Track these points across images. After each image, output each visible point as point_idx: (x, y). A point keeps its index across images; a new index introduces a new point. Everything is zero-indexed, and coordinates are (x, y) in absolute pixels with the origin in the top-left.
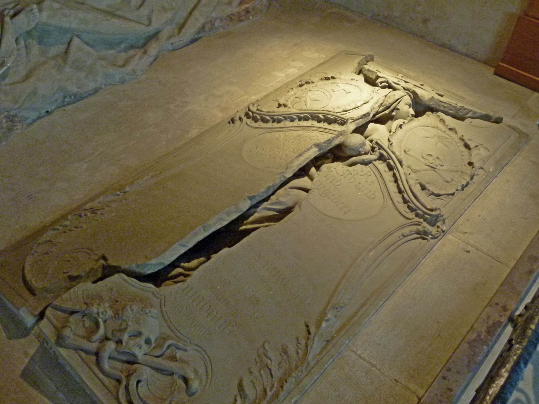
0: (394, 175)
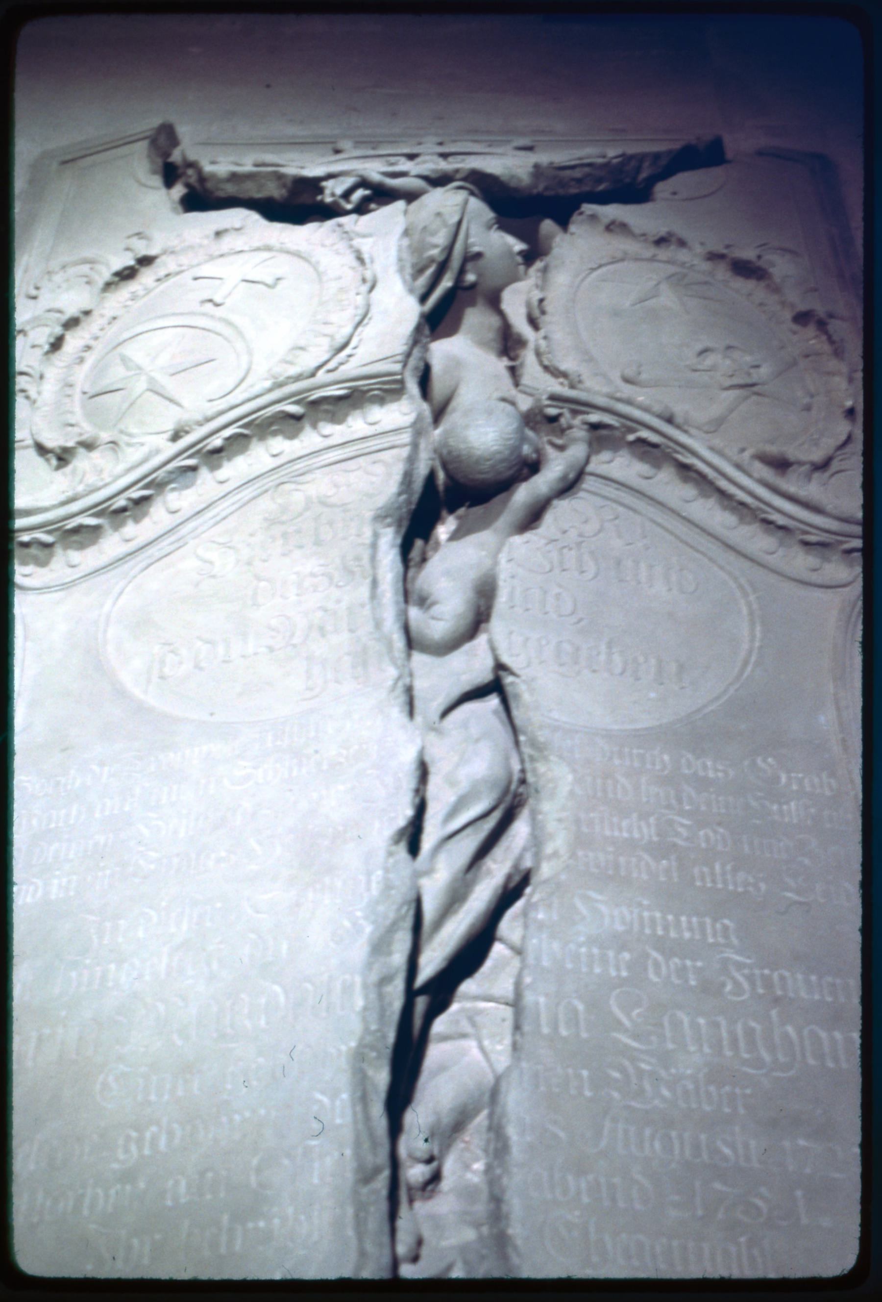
0: (684, 469)
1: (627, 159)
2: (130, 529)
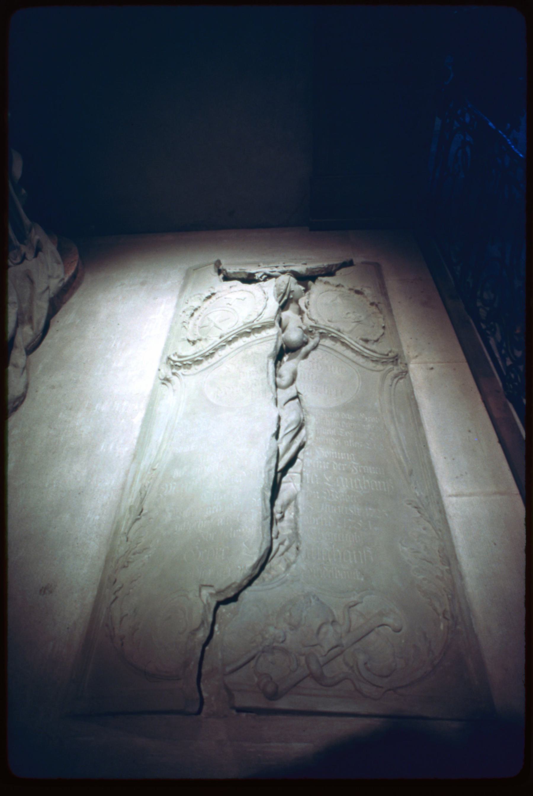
0: (343, 343)
1: (329, 266)
2: (210, 360)
